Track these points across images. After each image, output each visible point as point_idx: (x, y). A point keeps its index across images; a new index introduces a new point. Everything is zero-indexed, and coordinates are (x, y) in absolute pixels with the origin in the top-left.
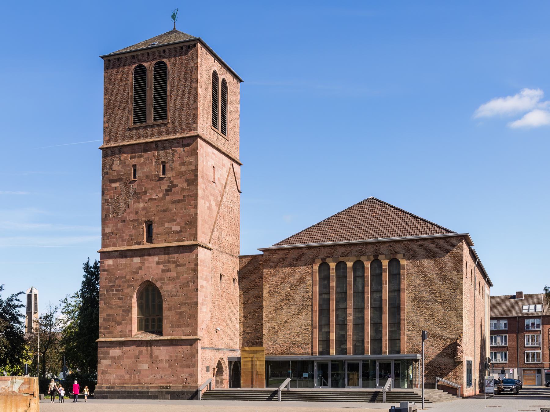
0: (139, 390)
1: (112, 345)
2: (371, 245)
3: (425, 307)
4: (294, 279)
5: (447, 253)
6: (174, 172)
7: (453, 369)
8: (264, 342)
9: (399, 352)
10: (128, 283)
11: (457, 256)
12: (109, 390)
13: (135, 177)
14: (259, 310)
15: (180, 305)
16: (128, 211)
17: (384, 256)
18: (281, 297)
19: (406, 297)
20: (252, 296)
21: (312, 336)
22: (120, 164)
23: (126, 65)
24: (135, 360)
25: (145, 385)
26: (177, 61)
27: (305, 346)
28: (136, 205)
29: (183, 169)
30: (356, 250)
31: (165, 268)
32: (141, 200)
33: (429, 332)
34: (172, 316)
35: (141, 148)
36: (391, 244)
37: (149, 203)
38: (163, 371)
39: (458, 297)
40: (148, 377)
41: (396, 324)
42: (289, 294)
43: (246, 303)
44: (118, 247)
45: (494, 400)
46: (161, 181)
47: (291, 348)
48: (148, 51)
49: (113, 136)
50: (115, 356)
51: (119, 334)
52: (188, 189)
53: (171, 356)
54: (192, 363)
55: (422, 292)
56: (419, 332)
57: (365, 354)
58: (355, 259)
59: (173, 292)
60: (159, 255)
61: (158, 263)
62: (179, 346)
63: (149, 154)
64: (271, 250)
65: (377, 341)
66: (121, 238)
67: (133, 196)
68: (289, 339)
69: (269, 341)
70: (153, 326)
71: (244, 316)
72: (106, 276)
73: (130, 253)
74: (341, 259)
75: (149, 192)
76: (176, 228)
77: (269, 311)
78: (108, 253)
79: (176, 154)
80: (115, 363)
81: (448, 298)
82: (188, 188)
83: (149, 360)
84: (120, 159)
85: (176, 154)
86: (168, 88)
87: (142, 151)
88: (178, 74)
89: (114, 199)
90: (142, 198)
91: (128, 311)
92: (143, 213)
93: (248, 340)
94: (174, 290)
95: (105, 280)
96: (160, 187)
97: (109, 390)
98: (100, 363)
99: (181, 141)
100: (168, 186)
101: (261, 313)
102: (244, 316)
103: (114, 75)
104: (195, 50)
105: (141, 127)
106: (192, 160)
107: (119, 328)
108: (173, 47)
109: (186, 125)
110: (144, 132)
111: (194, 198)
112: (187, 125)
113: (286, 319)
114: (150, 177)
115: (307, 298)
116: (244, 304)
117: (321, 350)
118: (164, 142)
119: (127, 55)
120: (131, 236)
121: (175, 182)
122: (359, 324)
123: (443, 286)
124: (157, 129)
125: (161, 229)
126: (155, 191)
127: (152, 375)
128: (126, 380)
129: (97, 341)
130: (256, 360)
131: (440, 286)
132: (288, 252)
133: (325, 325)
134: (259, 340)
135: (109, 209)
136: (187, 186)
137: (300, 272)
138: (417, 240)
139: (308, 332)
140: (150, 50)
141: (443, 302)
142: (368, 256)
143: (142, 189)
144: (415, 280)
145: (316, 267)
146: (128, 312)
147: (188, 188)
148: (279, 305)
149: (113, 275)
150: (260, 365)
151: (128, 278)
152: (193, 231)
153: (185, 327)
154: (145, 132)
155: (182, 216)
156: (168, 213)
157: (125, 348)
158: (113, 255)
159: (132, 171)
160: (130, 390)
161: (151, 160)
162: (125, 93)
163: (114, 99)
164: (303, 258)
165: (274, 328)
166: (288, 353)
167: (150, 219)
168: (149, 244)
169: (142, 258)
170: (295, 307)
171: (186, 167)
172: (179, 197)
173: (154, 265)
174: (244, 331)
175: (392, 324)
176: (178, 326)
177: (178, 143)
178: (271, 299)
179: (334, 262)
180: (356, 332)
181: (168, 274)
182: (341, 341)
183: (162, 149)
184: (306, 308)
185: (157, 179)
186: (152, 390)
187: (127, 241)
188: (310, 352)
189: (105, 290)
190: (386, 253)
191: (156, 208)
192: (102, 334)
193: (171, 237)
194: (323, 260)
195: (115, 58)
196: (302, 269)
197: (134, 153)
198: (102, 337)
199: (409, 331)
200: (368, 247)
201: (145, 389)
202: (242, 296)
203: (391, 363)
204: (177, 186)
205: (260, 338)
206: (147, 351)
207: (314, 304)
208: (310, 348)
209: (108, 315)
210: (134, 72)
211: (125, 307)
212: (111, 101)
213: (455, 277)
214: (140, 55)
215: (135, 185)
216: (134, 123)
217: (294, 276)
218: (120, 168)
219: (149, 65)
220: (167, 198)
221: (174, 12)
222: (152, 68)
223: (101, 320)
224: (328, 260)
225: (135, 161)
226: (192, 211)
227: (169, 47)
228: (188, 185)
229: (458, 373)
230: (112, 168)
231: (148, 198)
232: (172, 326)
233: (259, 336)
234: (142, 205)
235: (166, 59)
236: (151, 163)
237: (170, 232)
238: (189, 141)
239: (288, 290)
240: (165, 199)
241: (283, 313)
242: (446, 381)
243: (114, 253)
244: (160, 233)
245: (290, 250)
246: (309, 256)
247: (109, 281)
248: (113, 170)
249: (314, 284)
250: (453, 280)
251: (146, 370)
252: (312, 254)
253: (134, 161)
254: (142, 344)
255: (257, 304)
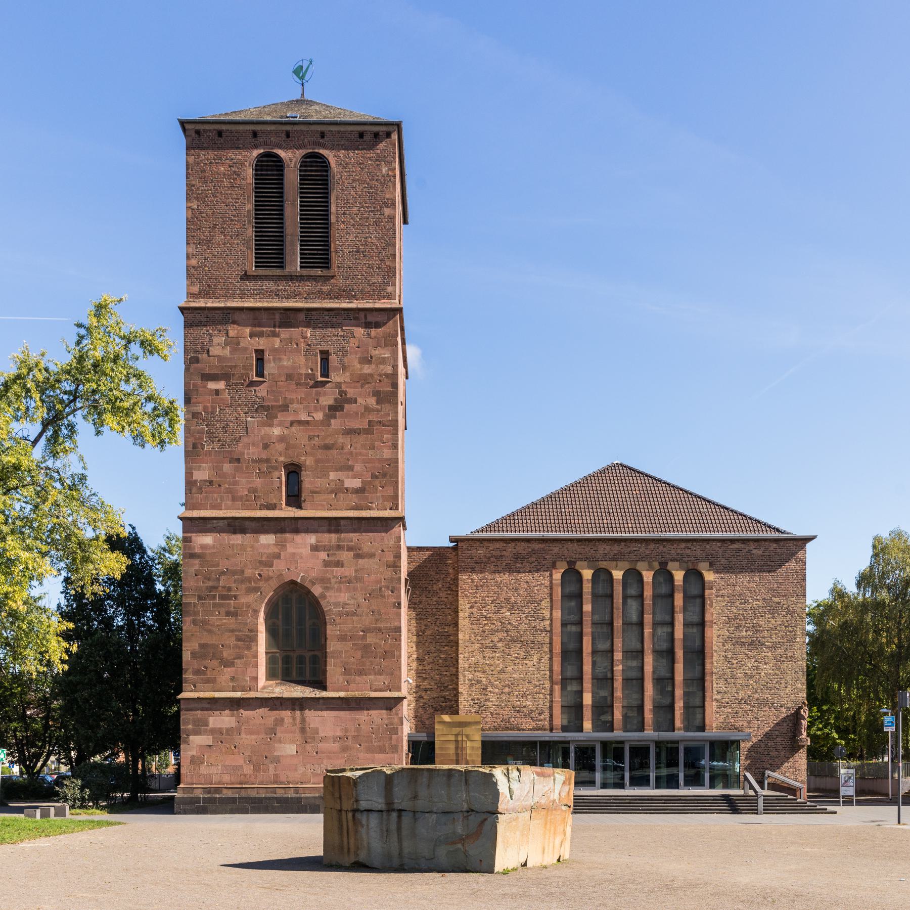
0: (278, 796)
1: (214, 707)
2: (655, 543)
3: (746, 654)
4: (516, 595)
5: (780, 566)
6: (348, 374)
7: (790, 758)
8: (461, 707)
9: (702, 728)
10: (248, 585)
11: (796, 572)
12: (209, 795)
13: (260, 373)
14: (446, 648)
15: (363, 631)
16: (245, 440)
17: (677, 564)
18: (492, 626)
19: (715, 635)
20: (432, 622)
21: (551, 698)
22: (226, 344)
23: (238, 148)
24: (266, 736)
25: (291, 786)
26: (351, 159)
27: (537, 715)
28: (263, 431)
29: (367, 369)
30: (629, 550)
31: (332, 559)
32: (275, 421)
33: (751, 696)
34: (346, 652)
35: (275, 318)
36: (689, 545)
37: (294, 429)
38: (329, 758)
39: (798, 640)
40: (296, 770)
41: (695, 681)
42: (507, 622)
43: (421, 634)
44: (225, 511)
45: (855, 807)
46: (319, 389)
47: (513, 719)
48: (288, 128)
49: (209, 286)
50: (220, 728)
51: (230, 684)
52: (378, 411)
53: (346, 730)
54: (391, 743)
55: (741, 628)
56: (736, 695)
57: (645, 732)
58: (627, 566)
59: (349, 606)
60: (317, 532)
61: (315, 548)
62: (364, 710)
63: (295, 332)
64: (472, 540)
65: (665, 709)
66: (231, 492)
67: (256, 410)
68: (509, 702)
69: (470, 705)
70: (301, 672)
71: (417, 658)
72: (197, 567)
73: (253, 525)
74: (603, 564)
75: (293, 407)
76: (356, 483)
77: (470, 650)
78: (201, 521)
79: (352, 340)
80: (222, 742)
81: (782, 641)
82: (379, 407)
83: (298, 736)
84: (227, 335)
85: (352, 340)
86: (333, 208)
87: (277, 324)
88: (354, 184)
89: (213, 412)
90: (276, 417)
91: (248, 640)
92: (280, 447)
93: (425, 703)
94: (352, 602)
95: (196, 575)
96: (317, 401)
97: (209, 795)
98: (187, 742)
99: (362, 315)
100: (335, 399)
101: (449, 655)
102: (418, 659)
103: (210, 163)
104: (391, 144)
105: (273, 276)
106: (386, 356)
107: (228, 672)
108: (342, 128)
109: (371, 285)
110: (278, 288)
111: (390, 428)
112: (374, 286)
113: (501, 666)
114: (295, 379)
115: (541, 631)
116: (418, 635)
117: (565, 723)
118: (326, 313)
119: (241, 128)
120: (254, 491)
121: (351, 393)
122: (632, 679)
123: (773, 621)
124: (308, 286)
125: (321, 483)
126: (306, 407)
127: (304, 765)
128: (246, 775)
129: (179, 697)
130: (465, 739)
131: (770, 620)
132: (505, 545)
133: (571, 679)
134: (446, 702)
135: (201, 432)
136: (375, 404)
137: (527, 582)
138: (733, 541)
139: (543, 691)
140: (292, 126)
141: (774, 647)
142: (649, 562)
143: (278, 401)
144: (729, 608)
145: (557, 576)
146: (250, 642)
147: (379, 407)
148: (487, 642)
149: (214, 566)
150: (473, 748)
151: (248, 573)
152: (390, 491)
153: (375, 674)
154: (281, 287)
155: (365, 462)
156: (334, 452)
157: (245, 713)
158: (215, 525)
159: (254, 363)
160: (257, 796)
161: (297, 345)
162: (236, 203)
163: (210, 212)
164: (534, 559)
165: (479, 682)
166: (508, 728)
167: (295, 460)
168: (294, 509)
169: (279, 535)
170: (519, 645)
171: (373, 366)
172: (360, 424)
173: (306, 551)
174: (417, 687)
175: (689, 681)
176: (361, 673)
177: (356, 318)
178: (473, 629)
179: (589, 568)
180: (627, 692)
181: (338, 571)
182: (603, 708)
183: (320, 325)
184: (539, 648)
185: (311, 384)
186: (307, 795)
187: (245, 501)
188: (548, 726)
189: (195, 595)
190: (680, 559)
191: (309, 441)
192: (189, 683)
193: (342, 499)
194: (571, 564)
195: (211, 128)
196: (531, 578)
197: (260, 326)
198: (189, 689)
199: (719, 693)
200: (649, 547)
201: (290, 794)
202: (414, 621)
203: (649, 747)
204: (355, 401)
205: (448, 699)
206: (294, 719)
207: (554, 641)
208: (548, 719)
209: (202, 646)
210: (256, 165)
211: (242, 631)
212: (204, 215)
213: (793, 606)
214: (270, 132)
215: (262, 391)
216: (256, 267)
217: (516, 589)
218: (227, 352)
219: (290, 157)
220: (333, 423)
221: (300, 63)
222: (296, 162)
223: (186, 655)
224: (579, 565)
225: (261, 343)
226: (387, 453)
227: (334, 128)
228: (377, 404)
229: (797, 764)
230: (208, 351)
231: (291, 418)
232: (347, 672)
233: (447, 695)
234: (277, 431)
235: (327, 151)
236: (298, 351)
237: (339, 489)
238: (380, 318)
239: (506, 614)
240: (329, 425)
241: (497, 655)
242: (782, 777)
243: (215, 521)
244: (317, 490)
245: (509, 543)
246: (544, 555)
247: (205, 578)
248: (211, 354)
249: (554, 607)
250: (790, 610)
251: (292, 756)
252: (551, 552)
253: (259, 343)
254: (281, 704)
255: (443, 637)
